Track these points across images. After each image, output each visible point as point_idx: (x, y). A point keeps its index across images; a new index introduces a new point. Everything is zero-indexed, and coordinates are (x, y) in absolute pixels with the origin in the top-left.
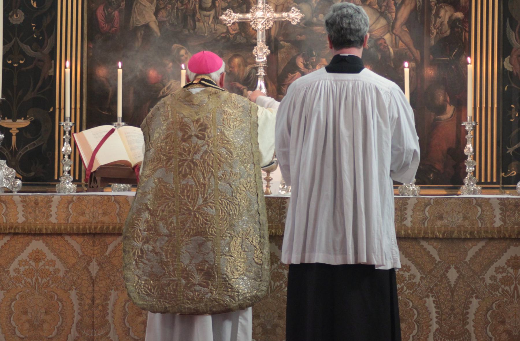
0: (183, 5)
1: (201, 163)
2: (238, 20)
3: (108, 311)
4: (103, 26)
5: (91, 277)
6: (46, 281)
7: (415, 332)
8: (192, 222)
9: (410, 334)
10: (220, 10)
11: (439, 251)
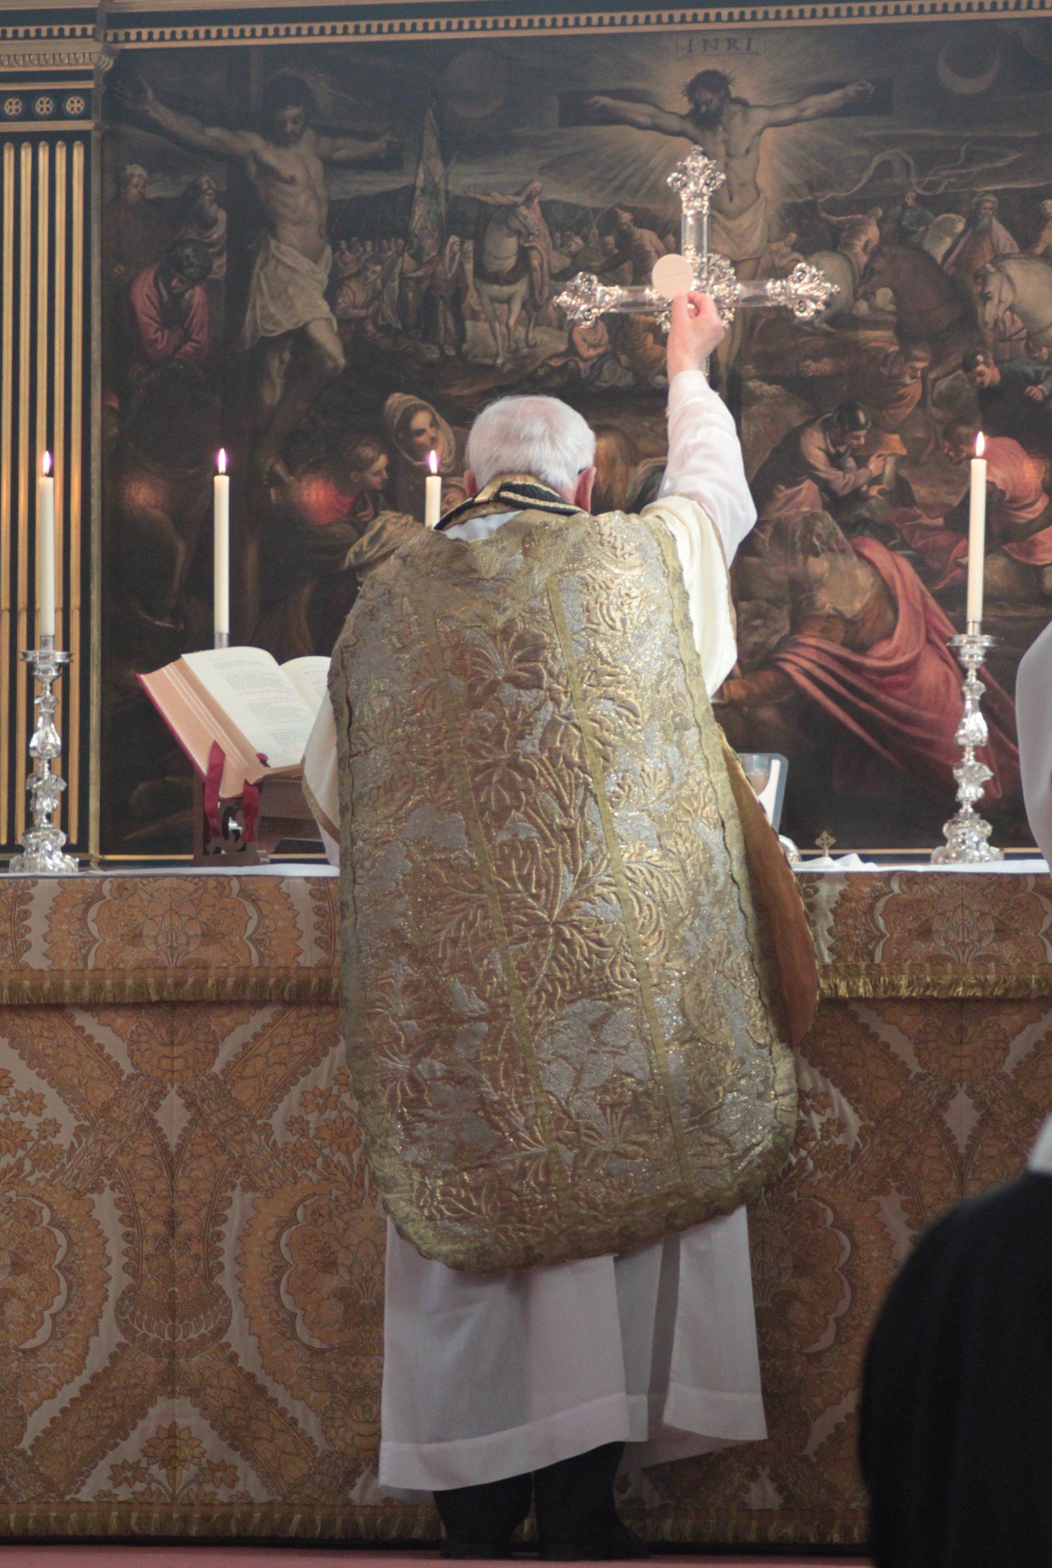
0: (420, 264)
1: (544, 765)
2: (614, 307)
3: (221, 1259)
4: (153, 337)
5: (165, 1148)
6: (13, 1161)
7: (59, 1302)
8: (555, 958)
9: (46, 1308)
10: (547, 279)
11: (133, 1042)
